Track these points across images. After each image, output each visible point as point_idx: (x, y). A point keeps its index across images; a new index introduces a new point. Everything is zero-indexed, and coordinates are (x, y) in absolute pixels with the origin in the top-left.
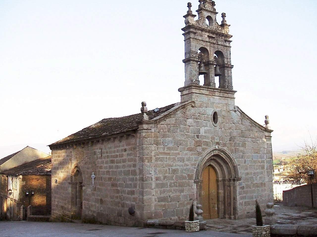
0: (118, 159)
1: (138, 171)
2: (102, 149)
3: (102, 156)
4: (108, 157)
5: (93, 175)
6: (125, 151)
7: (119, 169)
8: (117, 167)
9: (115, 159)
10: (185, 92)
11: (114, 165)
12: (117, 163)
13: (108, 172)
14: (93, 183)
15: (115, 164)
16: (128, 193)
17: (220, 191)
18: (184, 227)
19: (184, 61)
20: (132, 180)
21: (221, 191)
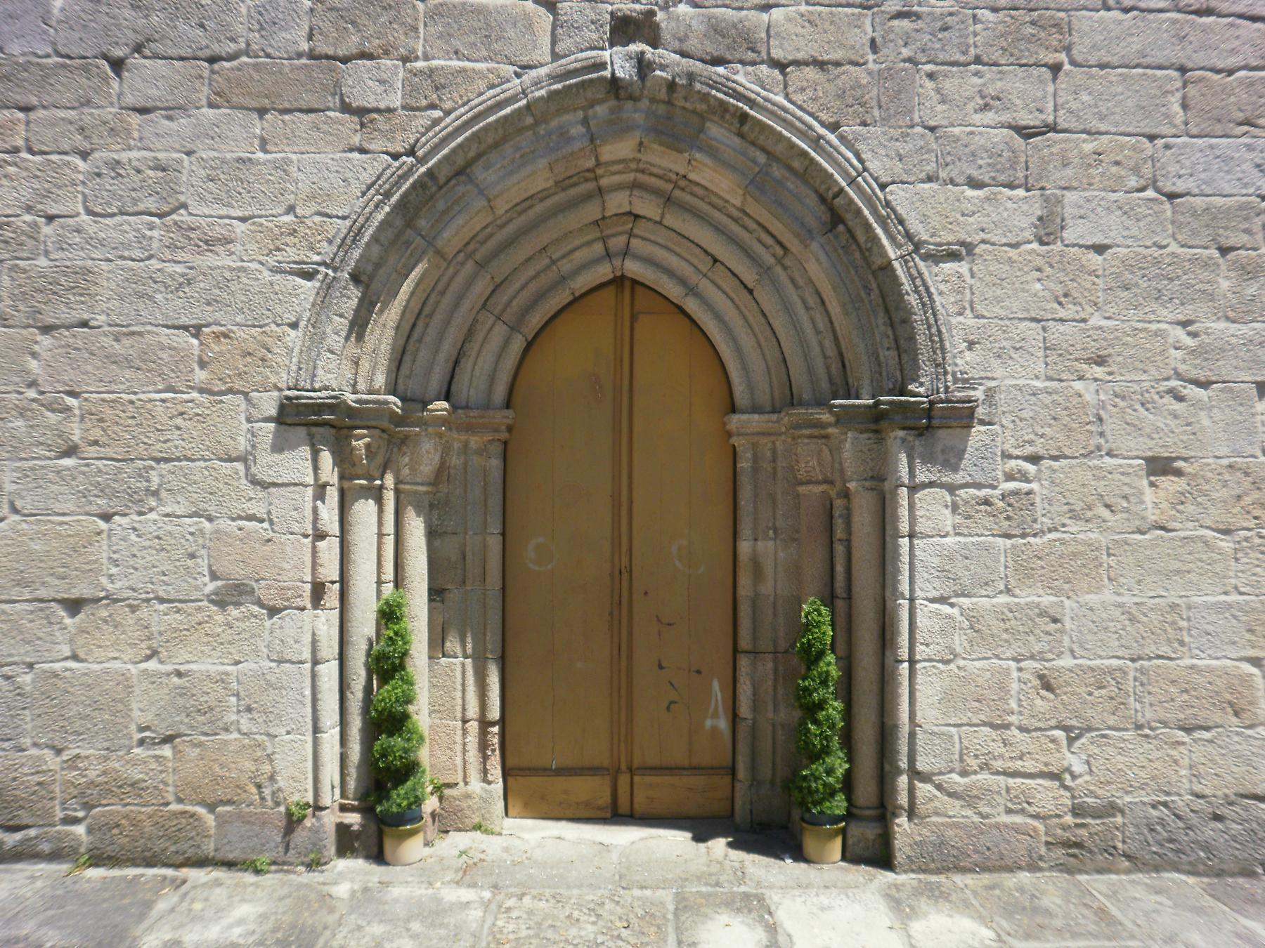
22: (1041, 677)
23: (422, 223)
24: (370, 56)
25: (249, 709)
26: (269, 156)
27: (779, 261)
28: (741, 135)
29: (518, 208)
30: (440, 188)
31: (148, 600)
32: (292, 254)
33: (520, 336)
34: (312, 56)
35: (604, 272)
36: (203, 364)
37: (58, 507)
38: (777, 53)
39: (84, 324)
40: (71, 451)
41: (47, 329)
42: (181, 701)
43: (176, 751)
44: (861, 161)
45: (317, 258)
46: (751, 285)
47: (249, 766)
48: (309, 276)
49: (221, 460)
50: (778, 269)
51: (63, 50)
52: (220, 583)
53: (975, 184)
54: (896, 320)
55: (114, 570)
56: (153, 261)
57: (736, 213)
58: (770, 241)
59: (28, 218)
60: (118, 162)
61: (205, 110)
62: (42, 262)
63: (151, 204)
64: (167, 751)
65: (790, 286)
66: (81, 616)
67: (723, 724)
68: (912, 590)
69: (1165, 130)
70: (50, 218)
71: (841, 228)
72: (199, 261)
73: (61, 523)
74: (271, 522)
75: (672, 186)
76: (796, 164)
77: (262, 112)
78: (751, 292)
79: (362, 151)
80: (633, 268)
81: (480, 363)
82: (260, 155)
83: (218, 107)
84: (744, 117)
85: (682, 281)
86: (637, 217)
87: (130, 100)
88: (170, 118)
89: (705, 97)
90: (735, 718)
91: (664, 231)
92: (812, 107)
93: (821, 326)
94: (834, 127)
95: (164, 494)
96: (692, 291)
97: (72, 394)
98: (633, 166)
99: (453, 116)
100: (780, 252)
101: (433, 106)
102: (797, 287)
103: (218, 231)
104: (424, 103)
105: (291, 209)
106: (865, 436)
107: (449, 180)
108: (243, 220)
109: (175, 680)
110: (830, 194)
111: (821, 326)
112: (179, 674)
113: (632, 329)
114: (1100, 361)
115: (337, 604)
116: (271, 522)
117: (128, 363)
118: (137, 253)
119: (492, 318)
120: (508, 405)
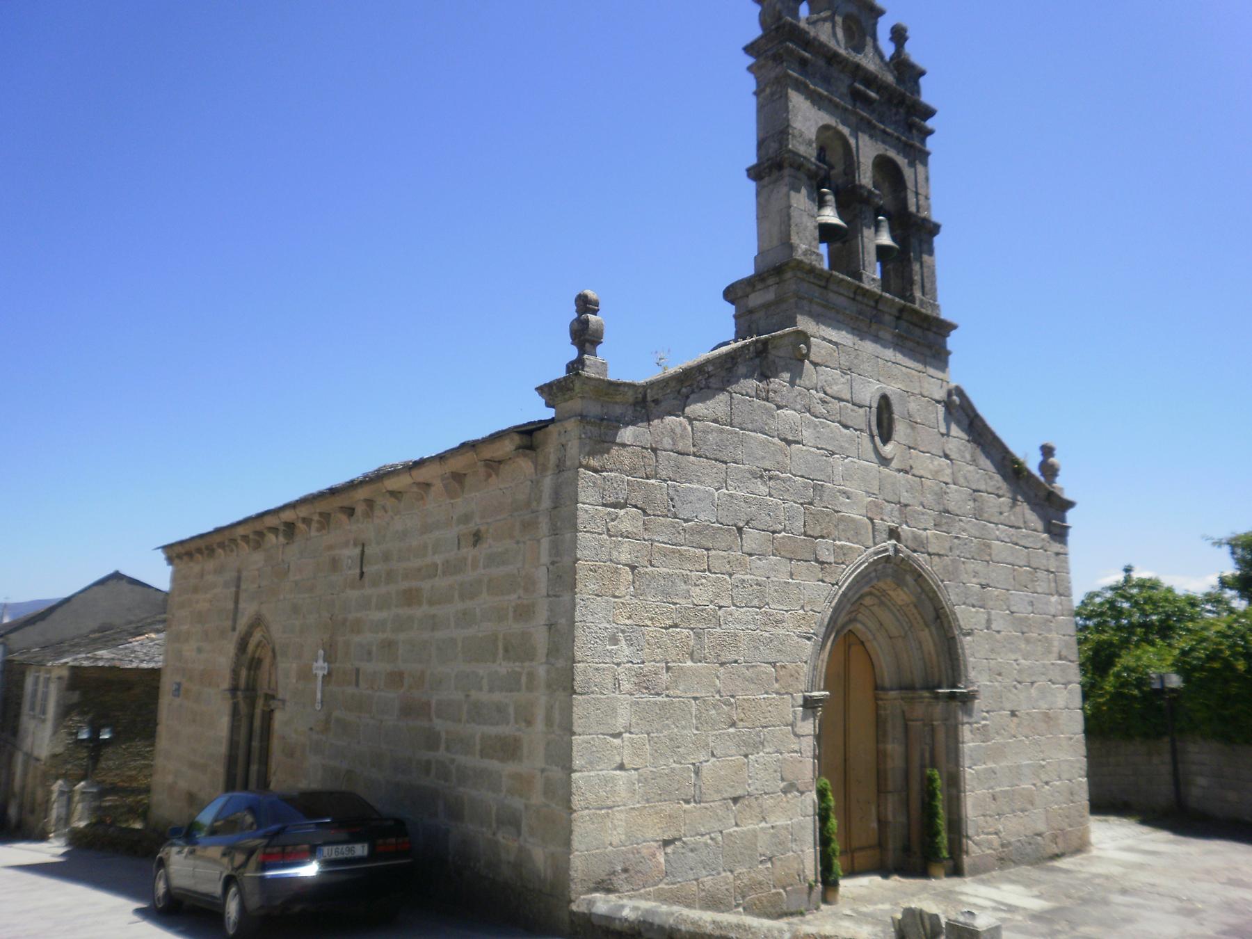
0: (441, 583)
1: (540, 639)
2: (363, 545)
3: (362, 574)
4: (390, 576)
5: (321, 663)
6: (475, 545)
7: (439, 634)
8: (433, 623)
9: (426, 585)
10: (756, 299)
11: (419, 612)
12: (431, 603)
13: (389, 645)
14: (319, 696)
15: (425, 608)
16: (481, 751)
17: (890, 747)
18: (177, 561)
19: (755, 173)
20: (511, 683)
21: (894, 748)
22: (993, 796)
25: (796, 840)
26: (794, 581)
28: (915, 580)
31: (761, 795)
32: (804, 629)
33: (893, 694)
34: (805, 534)
36: (777, 680)
37: (730, 753)
38: (930, 550)
39: (736, 662)
40: (733, 724)
41: (722, 664)
42: (774, 840)
43: (772, 863)
45: (812, 631)
47: (796, 866)
48: (809, 639)
49: (785, 726)
51: (721, 521)
52: (785, 783)
53: (974, 606)
55: (750, 782)
56: (758, 631)
59: (711, 606)
60: (744, 581)
61: (771, 557)
62: (718, 629)
63: (756, 602)
64: (769, 865)
66: (738, 805)
70: (720, 607)
71: (938, 621)
72: (774, 631)
73: (731, 760)
74: (801, 753)
76: (931, 595)
77: (791, 559)
79: (823, 581)
82: (790, 580)
83: (776, 556)
84: (920, 575)
87: (745, 549)
88: (759, 559)
89: (911, 565)
92: (937, 573)
94: (942, 581)
95: (765, 743)
97: (732, 696)
101: (843, 563)
103: (779, 617)
104: (841, 561)
105: (802, 607)
108: (787, 611)
109: (772, 831)
112: (773, 827)
114: (1000, 674)
116: (801, 753)
117: (751, 681)
118: (753, 627)
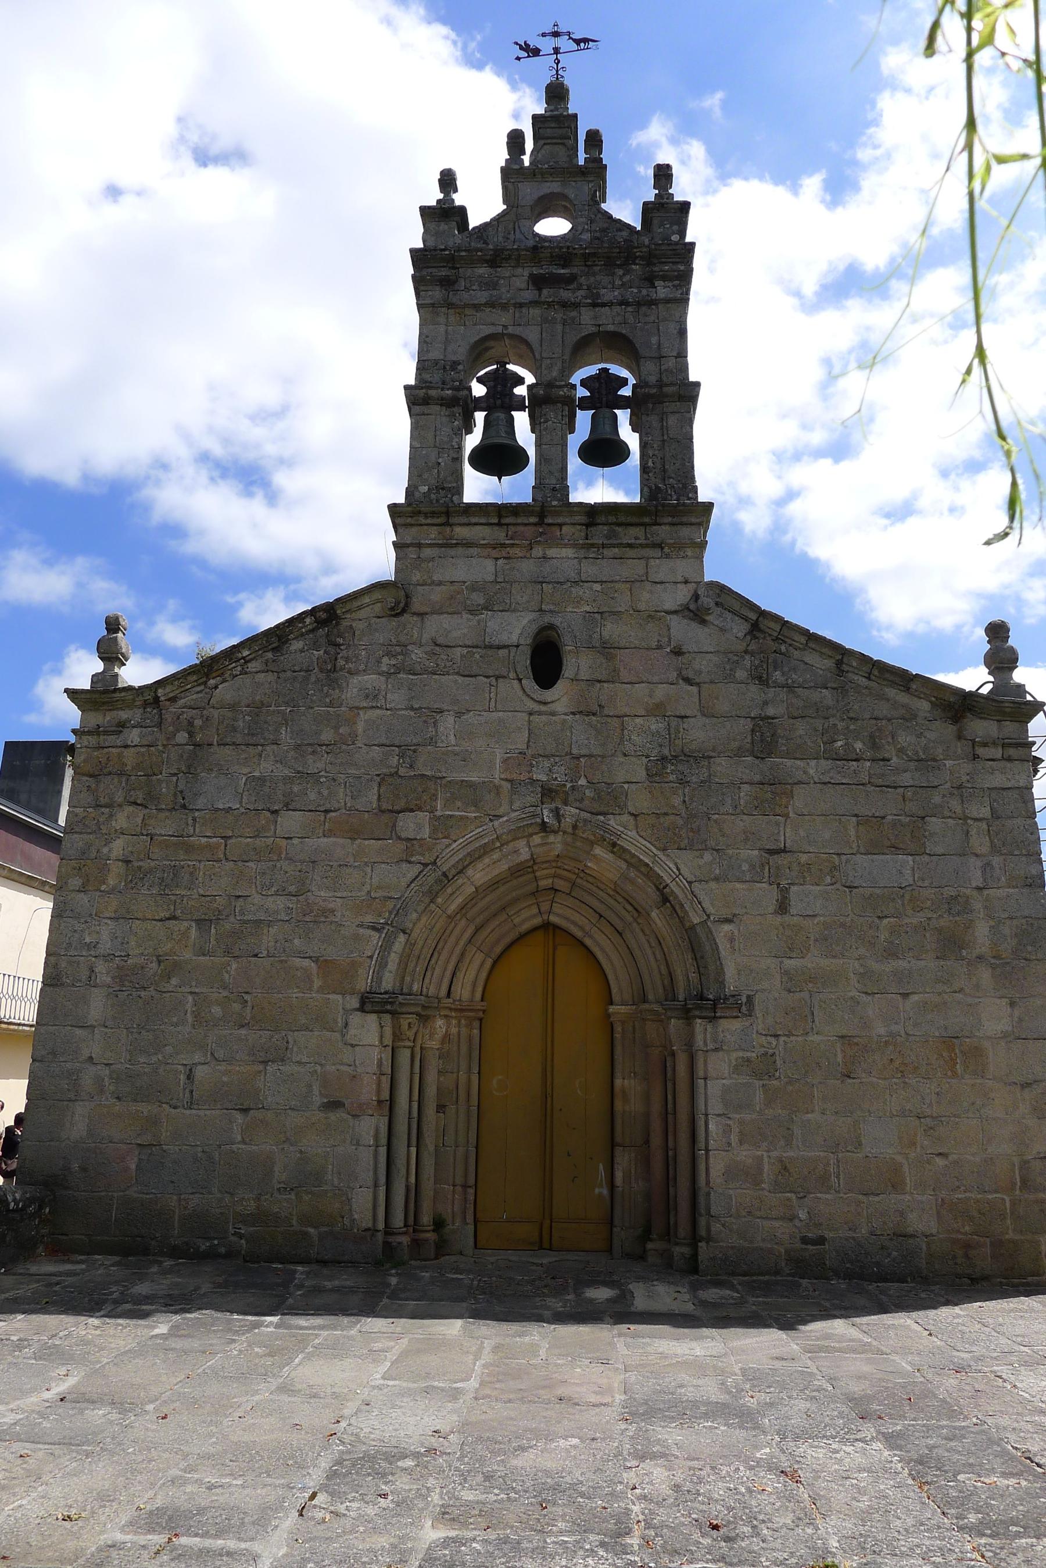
23: (439, 900)
24: (412, 811)
27: (635, 920)
29: (490, 889)
30: (449, 881)
35: (537, 921)
44: (678, 869)
46: (620, 930)
47: (337, 1205)
50: (635, 924)
54: (698, 956)
57: (612, 893)
58: (630, 908)
65: (641, 934)
67: (605, 1192)
68: (706, 1109)
69: (846, 851)
75: (575, 877)
76: (643, 869)
78: (620, 934)
80: (553, 919)
81: (468, 975)
85: (581, 928)
86: (556, 890)
90: (612, 1186)
91: (572, 899)
93: (659, 957)
96: (587, 934)
98: (554, 864)
99: (457, 843)
100: (636, 915)
102: (645, 934)
106: (681, 1021)
107: (454, 876)
110: (662, 887)
111: (659, 957)
113: (554, 954)
115: (388, 1114)
119: (475, 949)
120: (482, 1000)
